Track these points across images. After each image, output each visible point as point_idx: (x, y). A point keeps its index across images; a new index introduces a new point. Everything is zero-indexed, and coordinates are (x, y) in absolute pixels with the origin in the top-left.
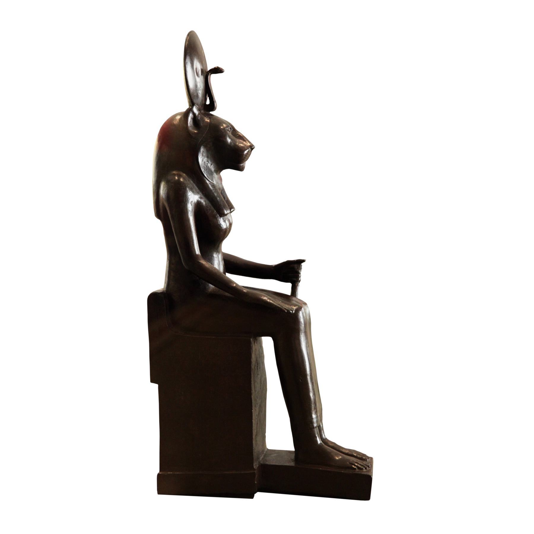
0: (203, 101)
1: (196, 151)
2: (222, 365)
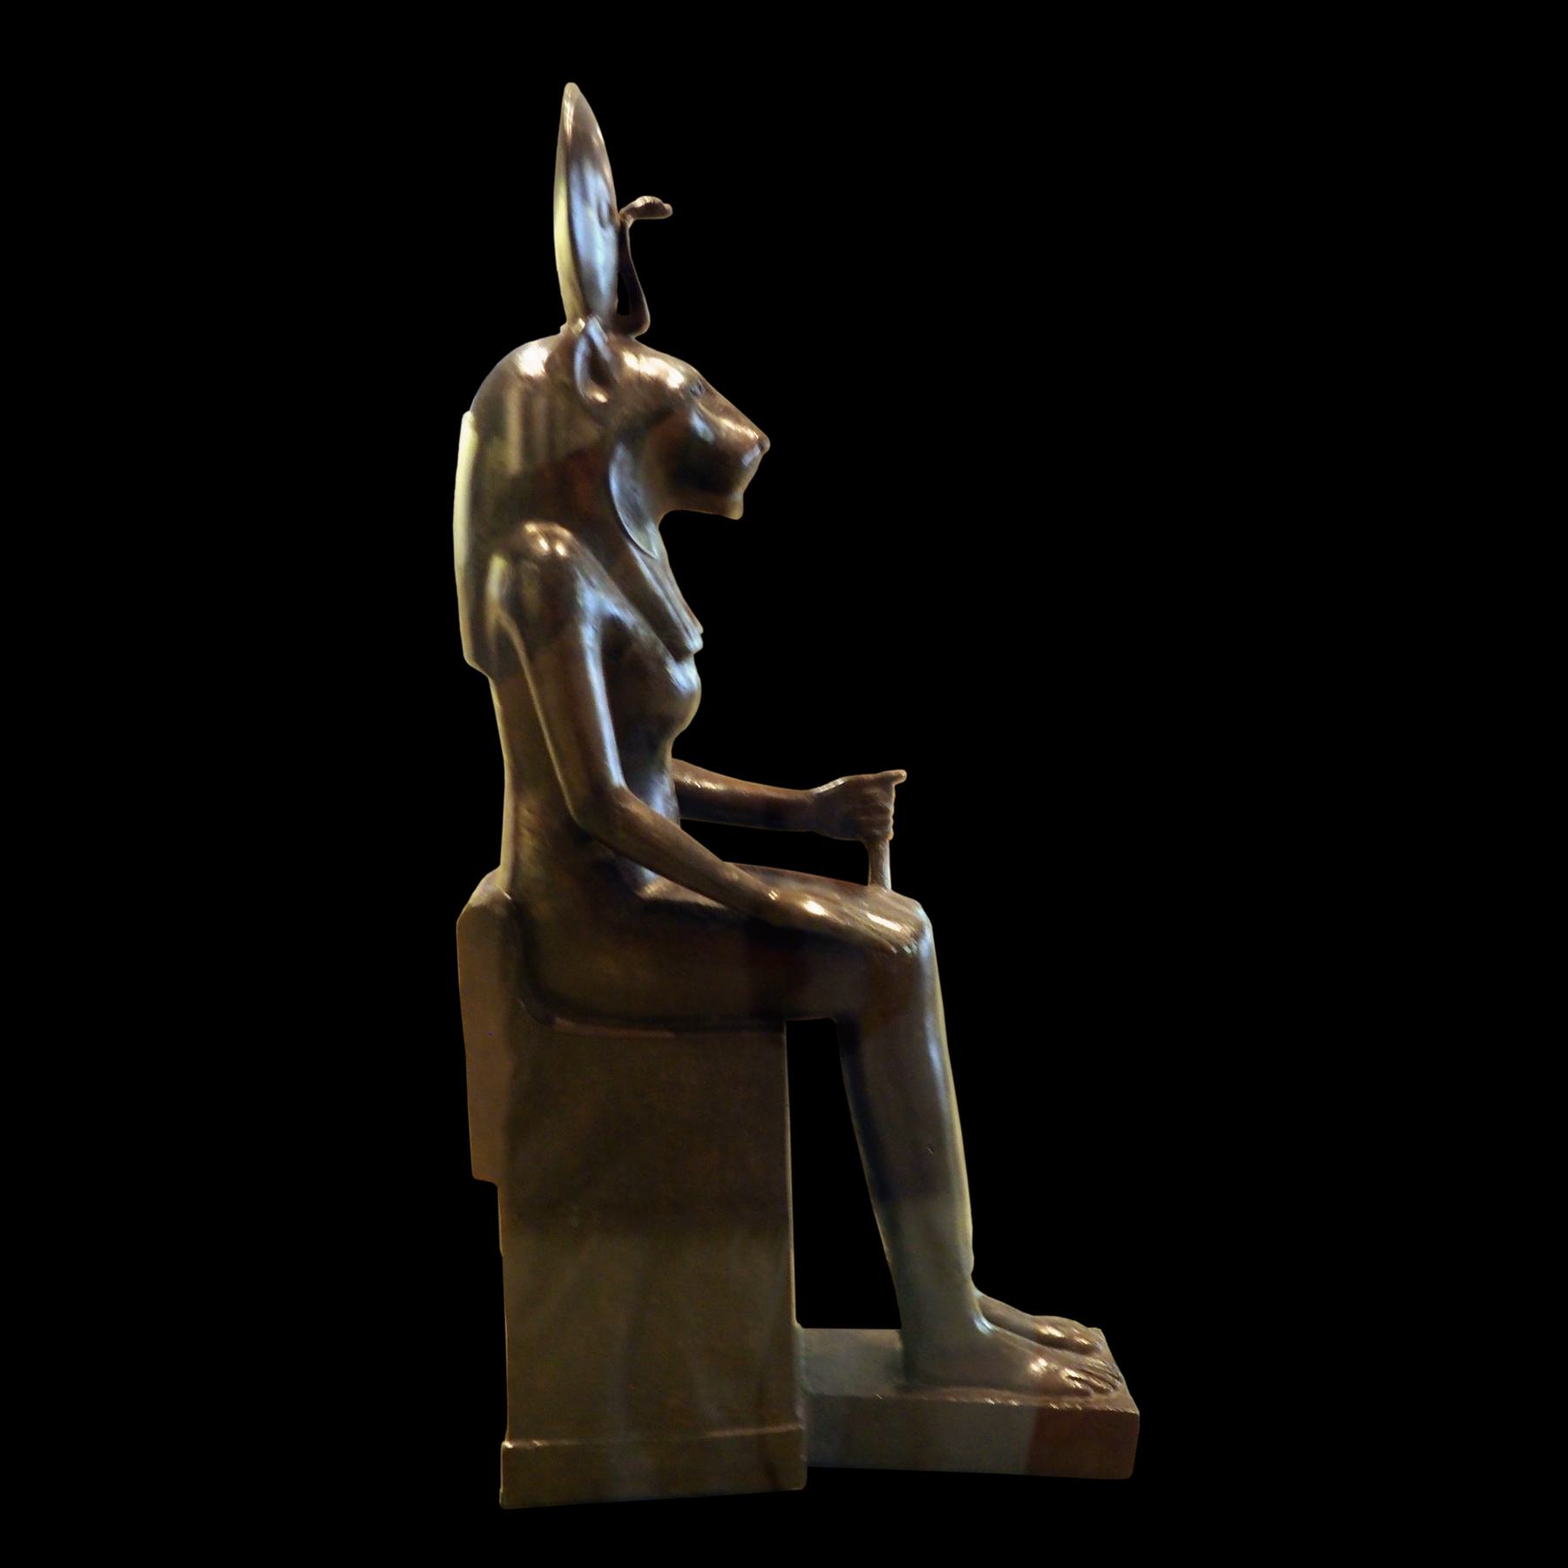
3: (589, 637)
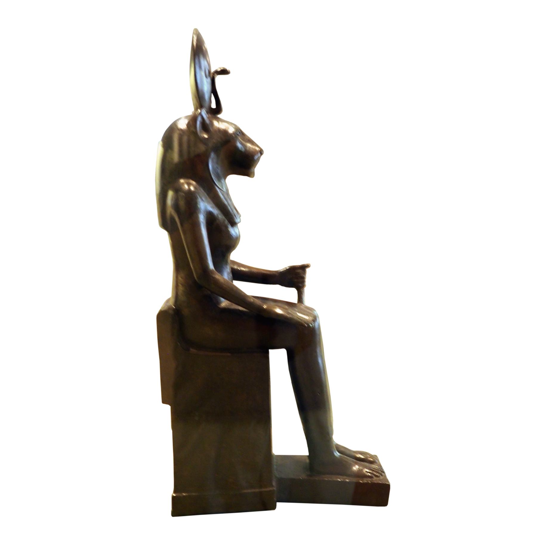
0: (208, 103)
1: (203, 161)
2: (229, 358)
3: (202, 218)
